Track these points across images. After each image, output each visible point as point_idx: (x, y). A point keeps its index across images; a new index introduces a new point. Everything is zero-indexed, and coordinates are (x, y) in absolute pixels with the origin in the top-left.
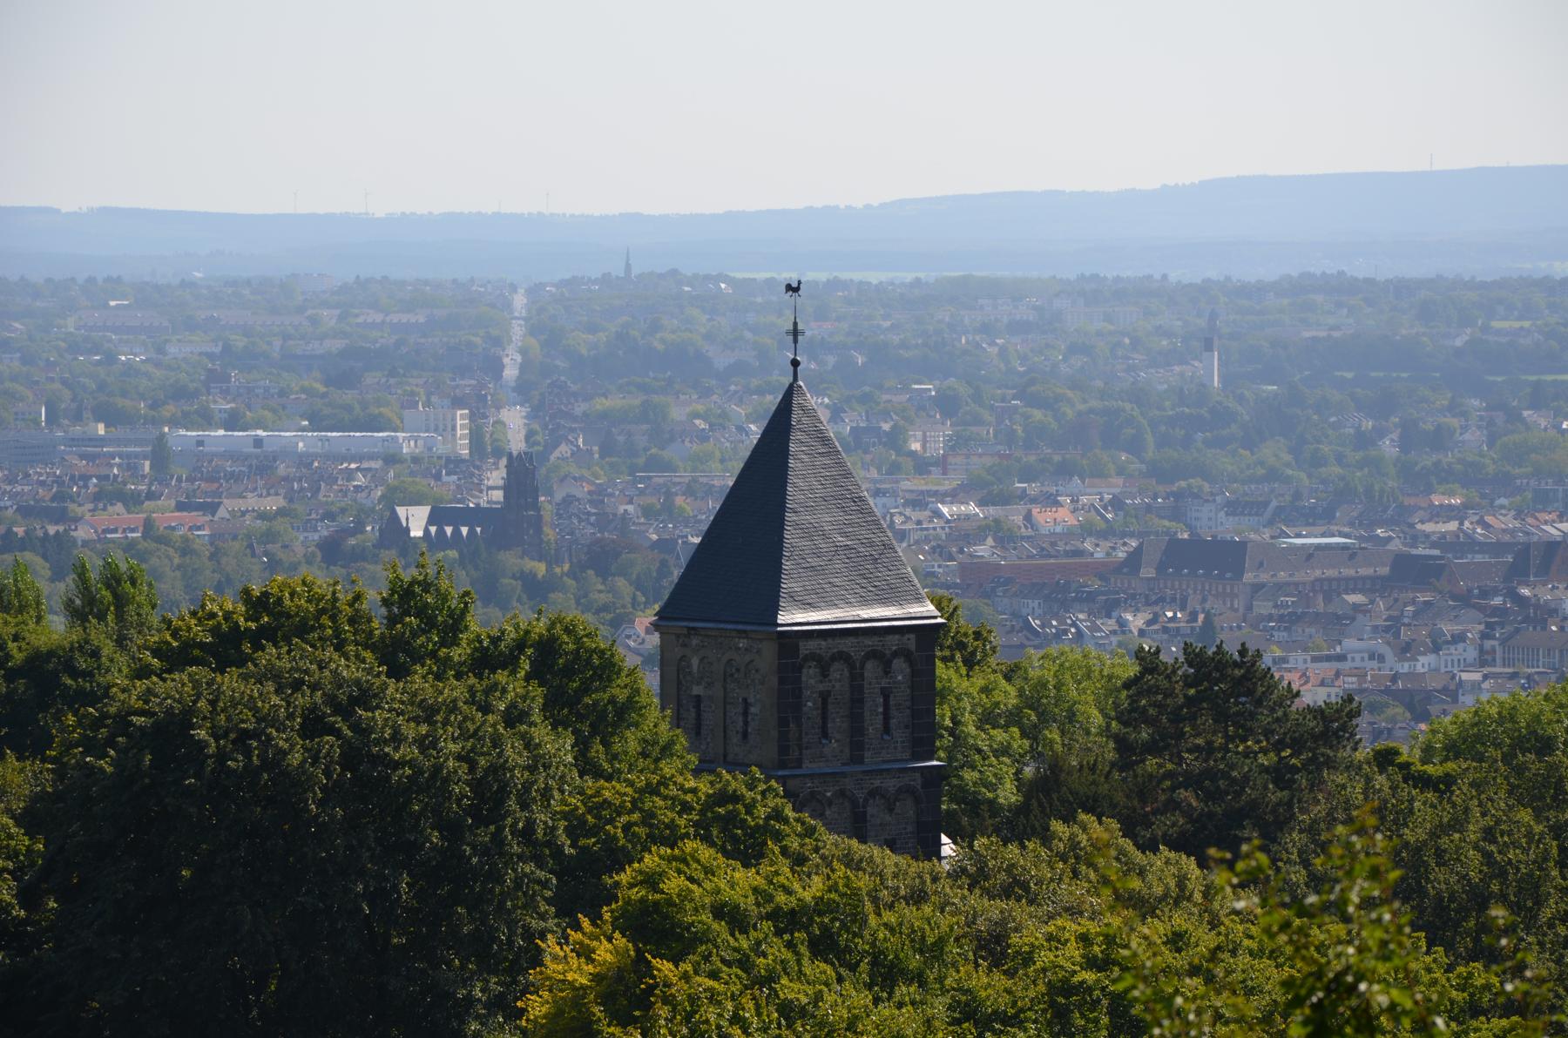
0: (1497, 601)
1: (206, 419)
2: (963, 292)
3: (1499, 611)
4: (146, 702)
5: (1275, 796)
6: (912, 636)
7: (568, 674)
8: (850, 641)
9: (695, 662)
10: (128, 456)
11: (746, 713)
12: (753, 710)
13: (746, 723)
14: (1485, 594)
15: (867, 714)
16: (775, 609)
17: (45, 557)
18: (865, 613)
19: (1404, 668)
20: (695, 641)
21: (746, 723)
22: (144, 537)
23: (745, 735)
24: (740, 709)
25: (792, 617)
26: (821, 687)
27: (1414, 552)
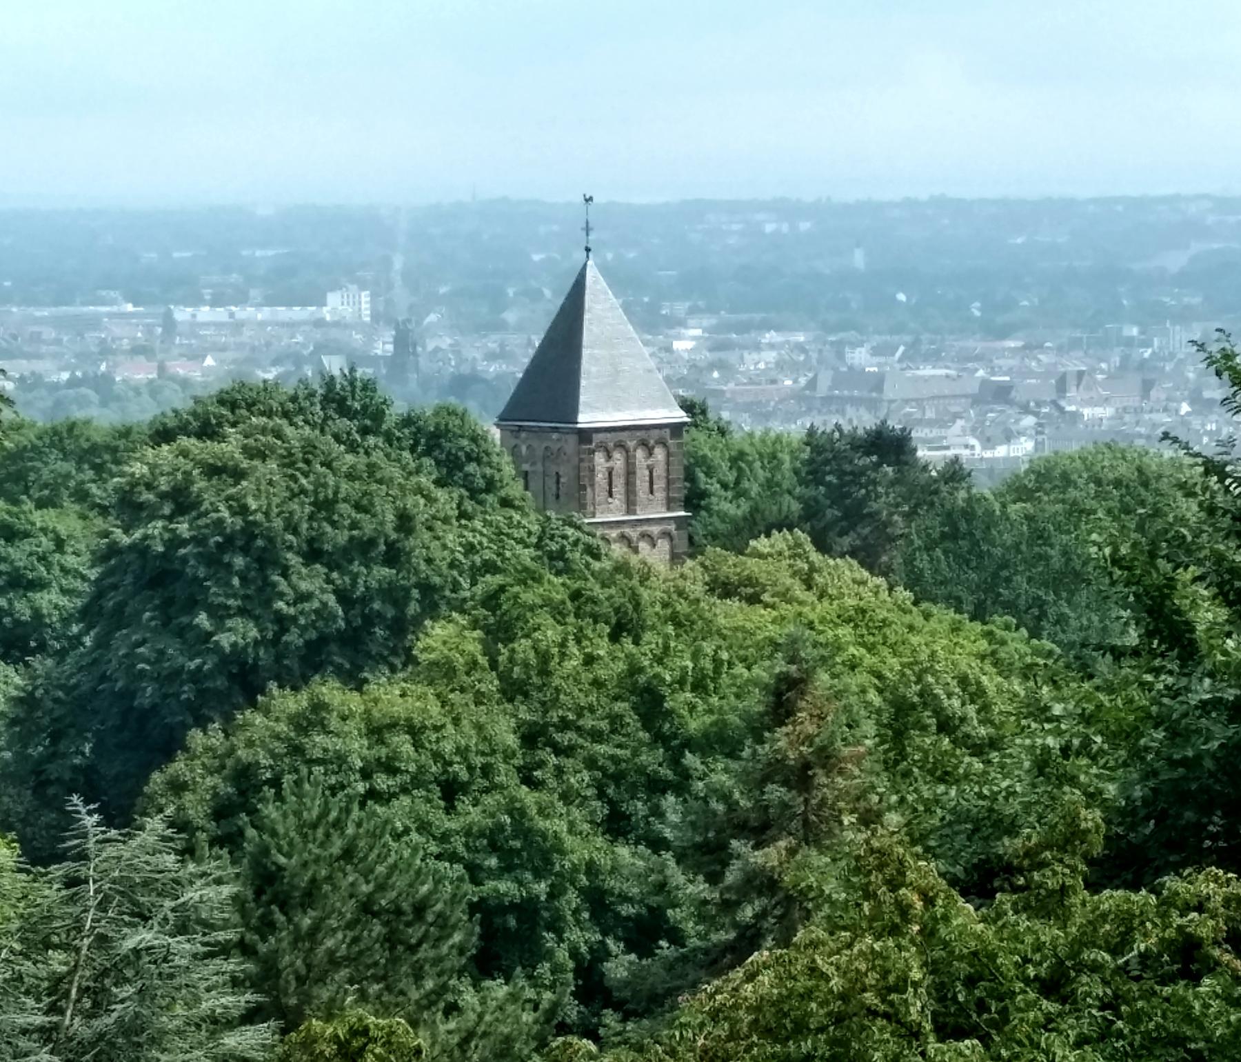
0: (1045, 410)
1: (197, 301)
2: (695, 210)
3: (1047, 415)
4: (580, 716)
5: (669, 611)
6: (668, 430)
7: (440, 445)
8: (626, 434)
9: (524, 449)
10: (148, 325)
11: (558, 482)
12: (562, 480)
13: (558, 489)
14: (1038, 405)
15: (638, 482)
16: (575, 411)
17: (97, 392)
18: (641, 414)
19: (988, 454)
20: (523, 435)
21: (558, 489)
22: (160, 376)
23: (558, 497)
24: (554, 480)
25: (586, 419)
26: (608, 465)
27: (993, 378)
